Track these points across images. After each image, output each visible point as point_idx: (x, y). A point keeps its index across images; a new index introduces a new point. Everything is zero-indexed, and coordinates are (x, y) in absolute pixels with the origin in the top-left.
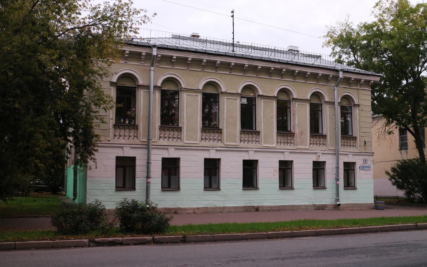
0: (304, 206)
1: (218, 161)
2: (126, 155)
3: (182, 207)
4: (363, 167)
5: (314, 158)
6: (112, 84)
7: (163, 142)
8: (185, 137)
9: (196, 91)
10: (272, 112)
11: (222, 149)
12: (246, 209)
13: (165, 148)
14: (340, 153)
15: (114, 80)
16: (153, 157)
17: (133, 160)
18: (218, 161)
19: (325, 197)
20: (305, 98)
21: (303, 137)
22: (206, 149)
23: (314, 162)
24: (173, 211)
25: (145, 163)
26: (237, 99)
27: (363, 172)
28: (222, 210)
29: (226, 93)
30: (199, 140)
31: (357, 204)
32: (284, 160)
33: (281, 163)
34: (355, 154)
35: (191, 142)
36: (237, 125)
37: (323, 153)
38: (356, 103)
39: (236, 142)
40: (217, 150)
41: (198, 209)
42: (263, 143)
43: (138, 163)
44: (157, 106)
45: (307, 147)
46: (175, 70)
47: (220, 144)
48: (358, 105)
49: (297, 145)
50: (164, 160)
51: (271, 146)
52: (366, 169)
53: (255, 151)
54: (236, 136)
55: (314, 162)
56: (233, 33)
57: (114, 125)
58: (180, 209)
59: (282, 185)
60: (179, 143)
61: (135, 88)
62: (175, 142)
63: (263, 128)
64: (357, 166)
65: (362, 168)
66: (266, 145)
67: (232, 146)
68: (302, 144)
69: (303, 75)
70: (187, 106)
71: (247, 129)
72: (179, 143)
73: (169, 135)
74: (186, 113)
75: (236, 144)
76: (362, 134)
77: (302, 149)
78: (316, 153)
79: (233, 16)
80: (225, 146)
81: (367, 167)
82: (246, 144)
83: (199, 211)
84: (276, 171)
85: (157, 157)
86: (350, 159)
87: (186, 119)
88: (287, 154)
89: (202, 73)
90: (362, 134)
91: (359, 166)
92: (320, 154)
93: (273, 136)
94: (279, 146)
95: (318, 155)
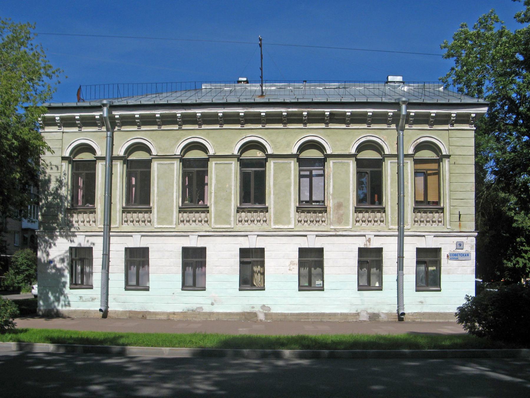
0: (341, 314)
1: (320, 251)
2: (311, 246)
3: (152, 310)
4: (455, 255)
5: (361, 243)
6: (64, 158)
7: (126, 227)
8: (156, 220)
9: (232, 156)
10: (289, 178)
11: (207, 234)
12: (244, 317)
13: (128, 234)
14: (102, 233)
15: (67, 154)
16: (406, 247)
17: (379, 251)
18: (320, 251)
19: (381, 302)
20: (347, 153)
21: (341, 212)
22: (185, 234)
23: (360, 250)
24: (140, 316)
25: (395, 255)
26: (232, 163)
27: (455, 263)
28: (144, 316)
29: (215, 157)
30: (174, 223)
31: (441, 313)
32: (307, 247)
33: (244, 252)
34: (145, 234)
35: (164, 226)
36: (231, 200)
37: (375, 236)
38: (444, 153)
39: (230, 224)
40: (199, 236)
41: (174, 313)
42: (272, 224)
43: (385, 255)
44: (118, 181)
45: (348, 227)
46: (143, 132)
47: (206, 227)
48: (448, 156)
49: (331, 224)
50: (420, 251)
51: (286, 227)
52: (460, 258)
53: (258, 236)
54: (229, 216)
55: (360, 250)
56: (261, 69)
57: (297, 208)
58: (149, 313)
59: (364, 282)
60: (148, 227)
61: (95, 161)
62: (143, 226)
63: (272, 202)
64: (444, 254)
65: (453, 257)
66: (277, 227)
67: (224, 230)
68: (339, 222)
69: (334, 118)
70: (158, 178)
71: (138, 205)
72: (148, 227)
73: (415, 217)
74: (158, 188)
75: (229, 226)
76: (455, 203)
77: (281, 230)
78: (364, 236)
79: (260, 45)
80: (213, 230)
81: (463, 255)
82: (246, 226)
83: (175, 316)
84: (294, 264)
85: (118, 247)
86: (430, 243)
87: (158, 196)
88: (311, 236)
89: (181, 132)
90: (455, 203)
91: (448, 253)
92: (372, 237)
93: (289, 213)
94: (300, 227)
95: (367, 239)
